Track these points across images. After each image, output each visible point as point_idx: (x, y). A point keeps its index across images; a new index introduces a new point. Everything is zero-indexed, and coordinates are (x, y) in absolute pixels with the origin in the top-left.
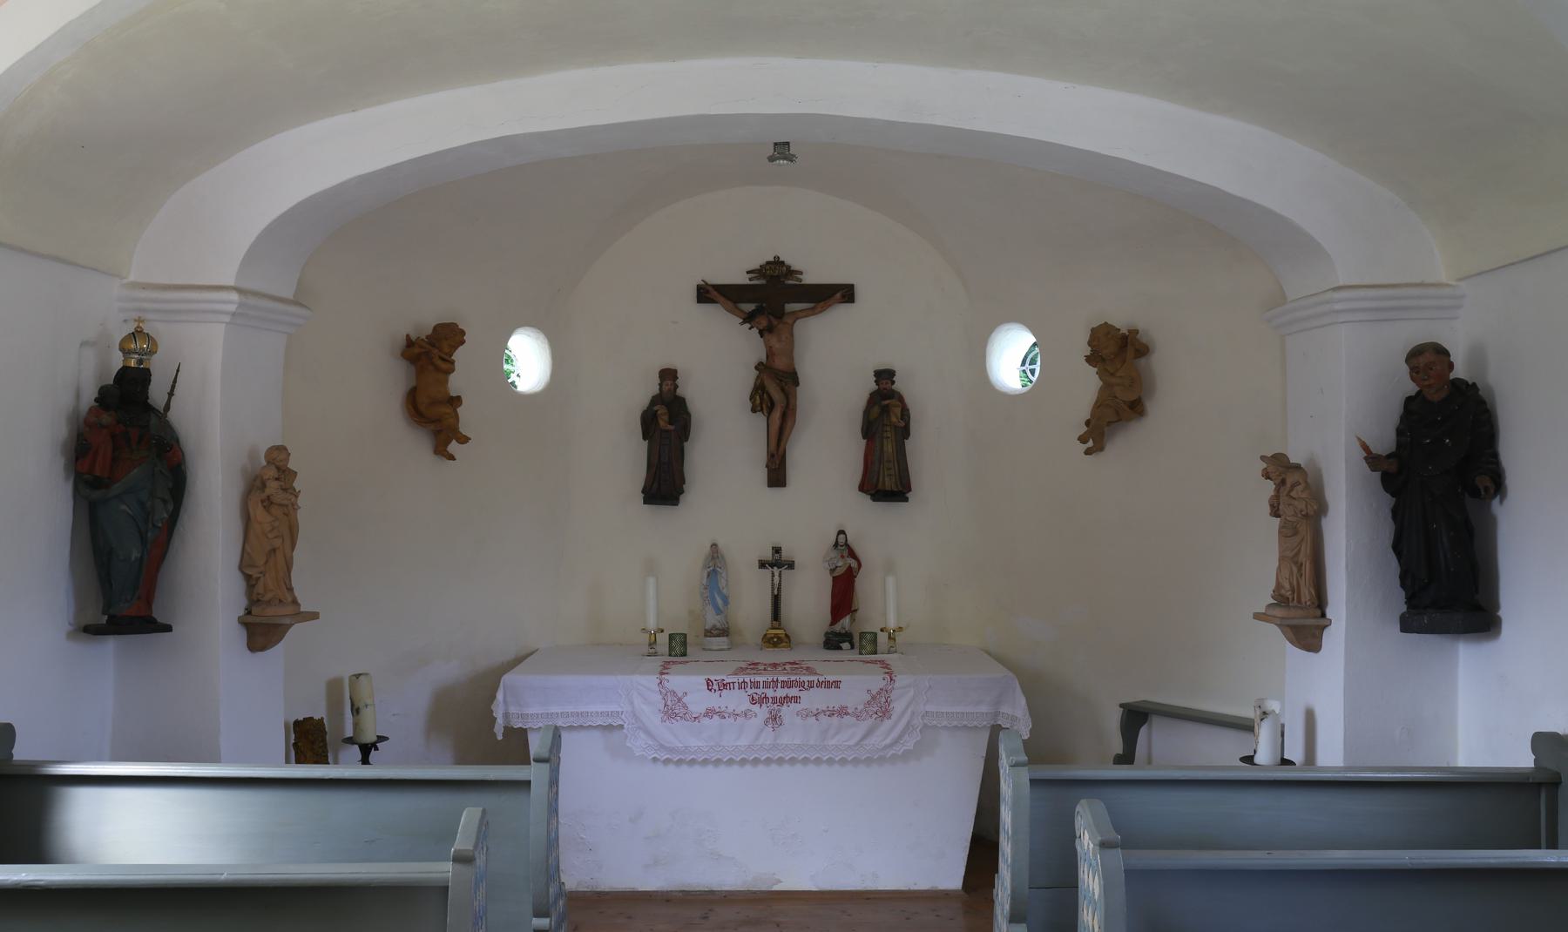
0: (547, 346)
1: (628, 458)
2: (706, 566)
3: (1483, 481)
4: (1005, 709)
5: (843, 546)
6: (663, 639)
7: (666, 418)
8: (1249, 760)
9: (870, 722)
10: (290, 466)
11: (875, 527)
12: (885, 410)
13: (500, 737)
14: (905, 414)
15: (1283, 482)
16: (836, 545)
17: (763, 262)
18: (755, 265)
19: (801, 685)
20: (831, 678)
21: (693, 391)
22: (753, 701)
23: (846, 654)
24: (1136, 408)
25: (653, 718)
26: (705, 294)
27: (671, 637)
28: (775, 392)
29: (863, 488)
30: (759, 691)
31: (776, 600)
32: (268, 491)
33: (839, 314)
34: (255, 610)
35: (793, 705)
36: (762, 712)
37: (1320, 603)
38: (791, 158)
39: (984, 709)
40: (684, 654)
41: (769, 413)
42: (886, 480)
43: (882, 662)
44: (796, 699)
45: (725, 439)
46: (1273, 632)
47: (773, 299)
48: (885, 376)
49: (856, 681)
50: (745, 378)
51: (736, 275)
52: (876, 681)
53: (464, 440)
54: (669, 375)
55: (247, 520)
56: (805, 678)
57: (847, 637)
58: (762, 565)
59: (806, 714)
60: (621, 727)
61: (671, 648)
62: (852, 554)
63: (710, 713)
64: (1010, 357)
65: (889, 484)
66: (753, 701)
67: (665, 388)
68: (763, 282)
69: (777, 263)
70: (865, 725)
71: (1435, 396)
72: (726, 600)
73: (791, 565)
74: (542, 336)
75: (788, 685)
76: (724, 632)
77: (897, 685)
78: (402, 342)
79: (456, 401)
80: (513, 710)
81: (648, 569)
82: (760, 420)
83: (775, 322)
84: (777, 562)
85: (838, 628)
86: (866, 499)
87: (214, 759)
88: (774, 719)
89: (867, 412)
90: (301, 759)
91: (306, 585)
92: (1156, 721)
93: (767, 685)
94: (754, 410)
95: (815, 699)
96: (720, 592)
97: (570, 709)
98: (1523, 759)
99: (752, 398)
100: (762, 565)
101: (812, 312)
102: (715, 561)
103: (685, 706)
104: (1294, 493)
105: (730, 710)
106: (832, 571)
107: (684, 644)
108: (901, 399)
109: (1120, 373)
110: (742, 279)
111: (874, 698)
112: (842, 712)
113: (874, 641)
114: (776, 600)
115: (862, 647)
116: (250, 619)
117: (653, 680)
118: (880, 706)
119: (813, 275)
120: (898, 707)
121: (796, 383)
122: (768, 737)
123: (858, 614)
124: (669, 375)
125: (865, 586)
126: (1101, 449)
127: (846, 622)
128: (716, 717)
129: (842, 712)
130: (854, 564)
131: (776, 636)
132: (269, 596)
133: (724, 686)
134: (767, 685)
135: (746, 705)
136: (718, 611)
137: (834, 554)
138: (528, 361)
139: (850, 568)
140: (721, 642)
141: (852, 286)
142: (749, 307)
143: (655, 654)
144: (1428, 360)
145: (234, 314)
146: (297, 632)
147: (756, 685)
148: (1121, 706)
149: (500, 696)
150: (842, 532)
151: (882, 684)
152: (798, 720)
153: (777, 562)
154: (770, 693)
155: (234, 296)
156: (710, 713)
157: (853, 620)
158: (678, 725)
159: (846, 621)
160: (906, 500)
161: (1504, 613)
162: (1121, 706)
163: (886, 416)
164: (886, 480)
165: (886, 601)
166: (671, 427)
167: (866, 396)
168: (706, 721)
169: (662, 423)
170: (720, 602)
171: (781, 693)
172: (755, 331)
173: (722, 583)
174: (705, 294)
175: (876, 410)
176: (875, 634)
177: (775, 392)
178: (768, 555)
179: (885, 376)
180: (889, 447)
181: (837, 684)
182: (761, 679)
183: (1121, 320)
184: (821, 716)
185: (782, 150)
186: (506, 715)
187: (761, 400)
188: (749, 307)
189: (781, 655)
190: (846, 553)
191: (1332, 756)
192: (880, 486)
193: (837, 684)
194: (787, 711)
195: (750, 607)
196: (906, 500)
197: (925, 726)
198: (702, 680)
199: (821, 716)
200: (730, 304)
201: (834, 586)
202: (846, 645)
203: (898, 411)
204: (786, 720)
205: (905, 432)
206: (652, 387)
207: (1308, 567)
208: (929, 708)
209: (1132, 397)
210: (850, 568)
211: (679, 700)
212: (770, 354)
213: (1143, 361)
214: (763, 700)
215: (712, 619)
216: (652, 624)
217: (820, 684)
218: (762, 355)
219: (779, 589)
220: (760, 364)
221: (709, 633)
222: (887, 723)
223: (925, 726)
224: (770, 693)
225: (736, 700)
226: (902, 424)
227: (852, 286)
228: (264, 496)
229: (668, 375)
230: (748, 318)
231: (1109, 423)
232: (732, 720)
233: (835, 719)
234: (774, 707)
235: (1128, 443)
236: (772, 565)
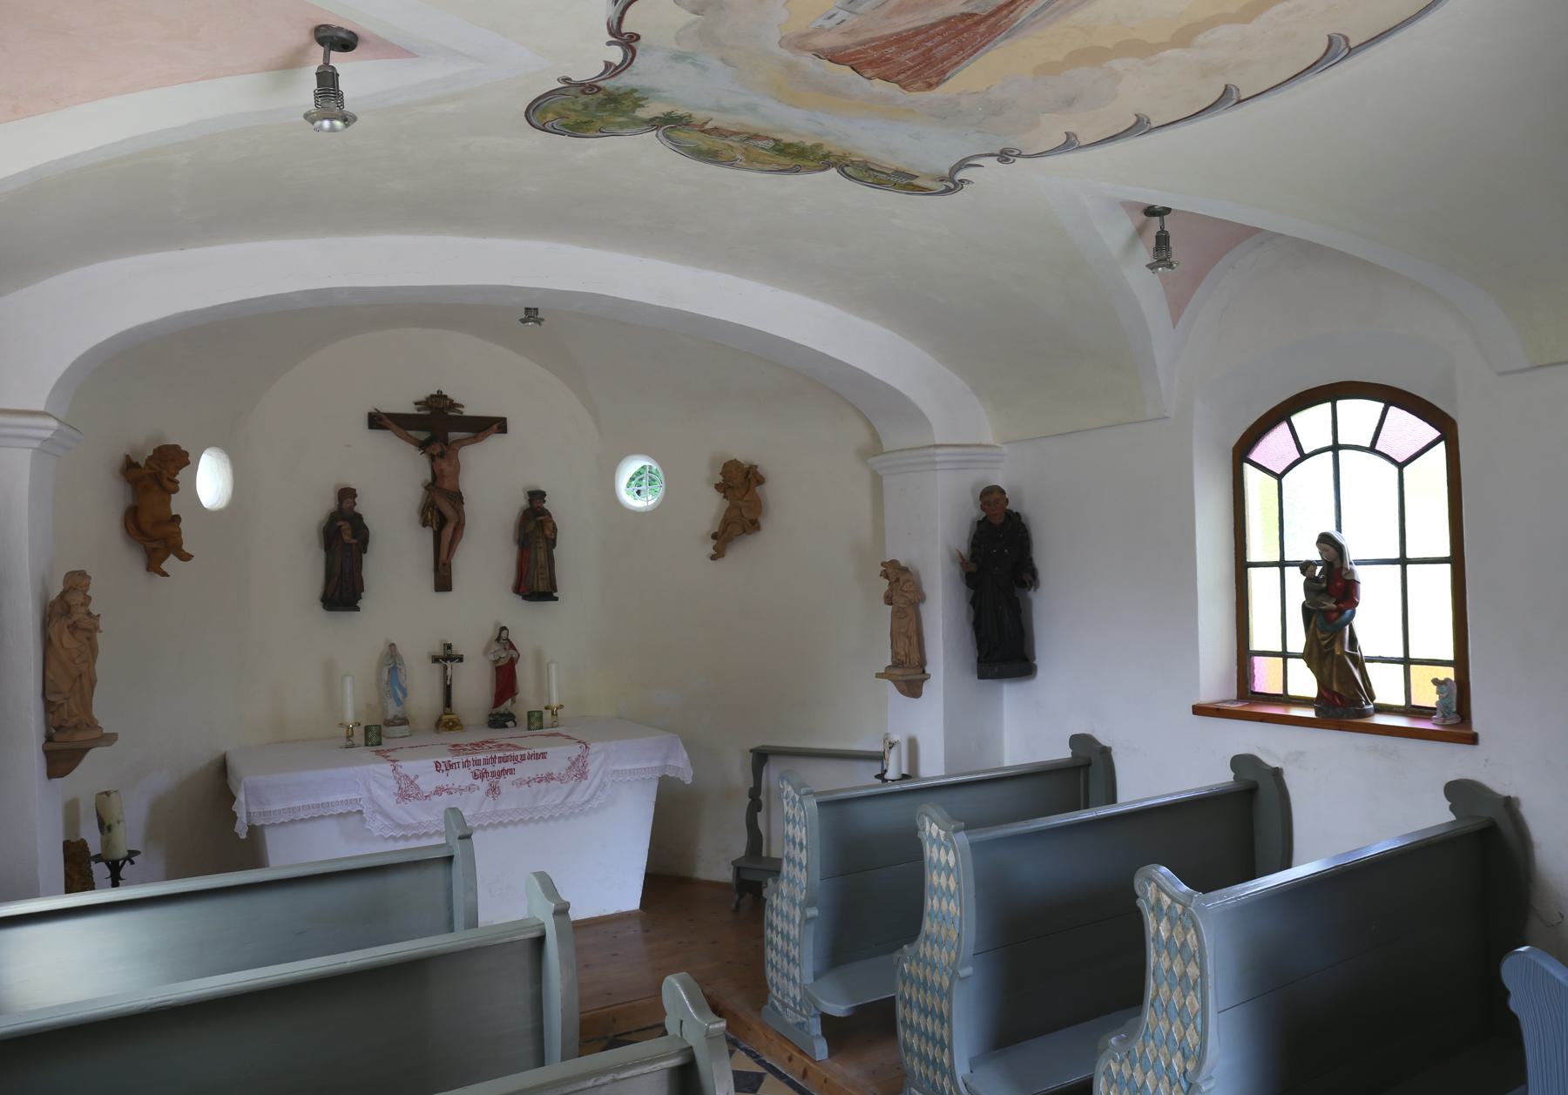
1: (306, 568)
3: (1027, 577)
5: (502, 637)
6: (359, 738)
8: (881, 776)
10: (545, 506)
11: (532, 627)
12: (541, 525)
13: (243, 836)
14: (555, 530)
15: (898, 580)
16: (498, 640)
18: (422, 397)
19: (515, 759)
20: (539, 751)
22: (475, 777)
24: (753, 526)
25: (387, 799)
26: (377, 421)
27: (367, 729)
28: (442, 513)
31: (448, 691)
32: (76, 617)
33: (494, 441)
34: (58, 737)
35: (509, 777)
36: (483, 785)
37: (922, 664)
38: (539, 321)
39: (656, 764)
42: (535, 580)
44: (511, 771)
45: (397, 551)
46: (889, 687)
47: (439, 428)
48: (536, 496)
51: (404, 404)
52: (574, 750)
53: (186, 557)
54: (346, 494)
55: (47, 643)
56: (518, 753)
58: (436, 659)
59: (522, 782)
62: (512, 647)
63: (439, 791)
65: (542, 587)
66: (475, 777)
69: (440, 396)
70: (566, 788)
71: (998, 521)
72: (405, 695)
73: (461, 659)
74: (224, 456)
75: (504, 760)
76: (404, 721)
78: (119, 460)
79: (177, 519)
80: (253, 809)
84: (447, 657)
85: (502, 709)
87: (33, 894)
88: (494, 790)
90: (70, 889)
91: (105, 709)
92: (772, 760)
93: (486, 762)
95: (526, 770)
96: (400, 686)
97: (311, 802)
98: (1064, 753)
101: (475, 440)
102: (392, 659)
103: (417, 787)
104: (901, 587)
109: (742, 496)
110: (411, 409)
112: (549, 778)
113: (541, 718)
114: (448, 691)
116: (51, 746)
119: (473, 407)
122: (489, 805)
124: (346, 494)
129: (549, 778)
132: (74, 720)
133: (450, 766)
134: (486, 762)
135: (469, 780)
136: (399, 703)
138: (211, 481)
141: (504, 419)
142: (423, 436)
143: (352, 746)
144: (991, 497)
145: (46, 440)
146: (93, 755)
147: (477, 763)
150: (504, 628)
153: (447, 657)
154: (489, 768)
155: (53, 424)
156: (439, 791)
158: (411, 805)
160: (358, 609)
161: (1037, 662)
163: (535, 528)
164: (535, 580)
168: (436, 798)
171: (499, 767)
173: (402, 678)
174: (377, 421)
175: (532, 525)
177: (442, 513)
178: (439, 651)
180: (542, 556)
181: (543, 755)
182: (481, 757)
183: (744, 455)
184: (534, 785)
185: (531, 315)
186: (249, 814)
188: (423, 436)
189: (499, 735)
191: (933, 768)
194: (504, 782)
196: (358, 609)
198: (430, 763)
202: (510, 724)
204: (503, 790)
205: (552, 543)
206: (330, 504)
207: (915, 639)
208: (616, 767)
212: (436, 476)
213: (758, 489)
214: (484, 774)
217: (530, 757)
218: (428, 476)
224: (489, 768)
225: (461, 777)
227: (504, 419)
228: (70, 622)
229: (346, 495)
230: (423, 446)
233: (543, 784)
234: (492, 779)
235: (743, 552)
236: (445, 660)
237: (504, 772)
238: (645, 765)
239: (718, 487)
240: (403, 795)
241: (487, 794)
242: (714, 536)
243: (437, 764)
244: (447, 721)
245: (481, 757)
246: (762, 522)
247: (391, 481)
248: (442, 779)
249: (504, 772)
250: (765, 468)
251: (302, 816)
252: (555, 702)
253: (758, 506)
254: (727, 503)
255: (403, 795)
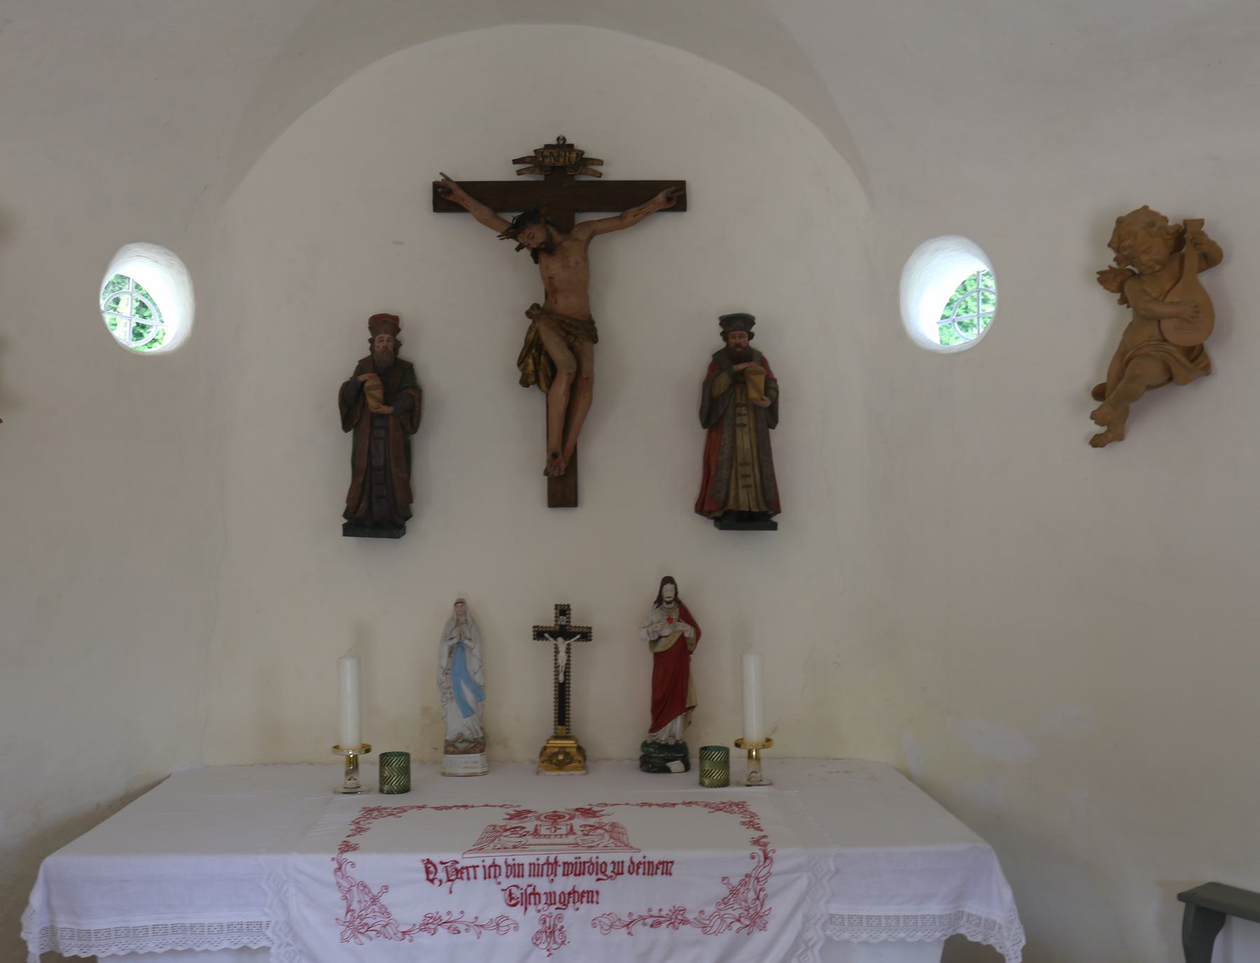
0: (185, 278)
1: (324, 462)
2: (447, 637)
4: (973, 908)
5: (671, 602)
6: (369, 772)
7: (378, 393)
9: (727, 936)
10: (753, 343)
12: (739, 380)
14: (771, 386)
16: (660, 601)
17: (540, 146)
19: (599, 869)
20: (656, 856)
21: (426, 352)
22: (511, 901)
23: (677, 785)
24: (1192, 363)
27: (385, 758)
28: (560, 355)
29: (702, 507)
30: (522, 882)
31: (562, 692)
33: (661, 230)
35: (584, 907)
36: (528, 920)
39: (934, 908)
40: (405, 789)
41: (549, 386)
42: (740, 497)
43: (741, 806)
44: (590, 896)
45: (478, 430)
47: (556, 204)
48: (737, 325)
49: (691, 839)
50: (509, 334)
51: (497, 167)
57: (679, 751)
58: (539, 634)
59: (611, 924)
60: (266, 949)
61: (383, 781)
62: (686, 616)
63: (431, 924)
64: (944, 293)
65: (746, 500)
66: (511, 901)
67: (380, 346)
68: (540, 178)
69: (562, 146)
72: (479, 692)
73: (586, 635)
74: (176, 262)
76: (477, 745)
77: (776, 867)
80: (63, 922)
81: (350, 639)
82: (534, 400)
83: (557, 237)
84: (564, 629)
85: (663, 736)
86: (706, 527)
88: (551, 933)
89: (708, 385)
93: (536, 870)
94: (524, 382)
95: (625, 896)
96: (470, 681)
97: (169, 919)
99: (521, 362)
100: (539, 634)
101: (621, 225)
103: (385, 912)
105: (469, 917)
106: (653, 643)
107: (405, 771)
108: (764, 362)
110: (506, 173)
111: (734, 892)
112: (677, 918)
113: (725, 763)
115: (703, 774)
117: (320, 865)
118: (746, 906)
119: (620, 167)
120: (779, 907)
121: (594, 338)
123: (694, 714)
124: (385, 326)
125: (708, 669)
126: (1120, 438)
127: (676, 726)
128: (442, 931)
129: (677, 918)
130: (689, 632)
131: (563, 750)
133: (457, 873)
134: (536, 870)
135: (498, 907)
136: (467, 711)
137: (657, 616)
139: (682, 640)
140: (473, 761)
148: (1181, 897)
149: (36, 898)
150: (668, 580)
151: (749, 867)
152: (595, 935)
153: (564, 629)
154: (542, 885)
156: (431, 924)
157: (687, 723)
159: (676, 725)
160: (774, 527)
162: (1181, 897)
163: (738, 391)
165: (741, 695)
166: (387, 410)
167: (707, 359)
168: (424, 939)
169: (372, 403)
170: (469, 696)
171: (563, 884)
172: (526, 252)
173: (473, 664)
175: (724, 380)
176: (726, 750)
177: (560, 355)
178: (549, 620)
179: (737, 325)
180: (745, 441)
181: (665, 867)
186: (50, 931)
187: (535, 366)
190: (675, 615)
192: (731, 505)
193: (665, 867)
194: (574, 918)
195: (521, 703)
196: (774, 527)
197: (829, 940)
198: (414, 862)
199: (637, 928)
200: (486, 211)
201: (656, 667)
202: (676, 765)
203: (760, 380)
204: (573, 933)
205: (770, 416)
209: (1190, 339)
210: (682, 640)
211: (375, 900)
212: (551, 290)
213: (1205, 279)
214: (528, 898)
215: (458, 724)
216: (350, 740)
217: (635, 868)
219: (567, 673)
220: (535, 306)
221: (452, 747)
222: (760, 938)
223: (829, 940)
224: (542, 885)
226: (767, 403)
230: (512, 232)
231: (1149, 387)
232: (472, 936)
233: (664, 932)
236: (555, 634)
237: (575, 896)
238: (909, 910)
239: (1105, 278)
240: (356, 926)
241: (536, 940)
242: (1099, 393)
243: (429, 867)
244: (565, 753)
245: (525, 859)
246: (1216, 354)
247: (466, 306)
248: (439, 900)
249: (575, 896)
250: (1222, 226)
251: (151, 946)
252: (754, 733)
253: (1203, 314)
254: (1127, 315)
255: (356, 926)
